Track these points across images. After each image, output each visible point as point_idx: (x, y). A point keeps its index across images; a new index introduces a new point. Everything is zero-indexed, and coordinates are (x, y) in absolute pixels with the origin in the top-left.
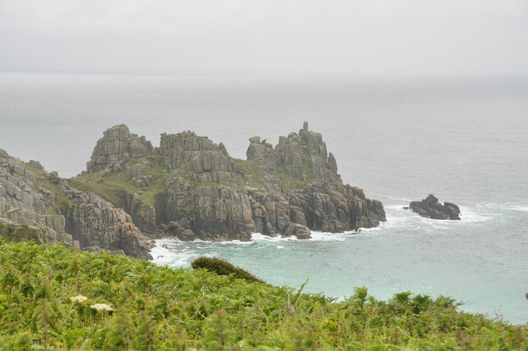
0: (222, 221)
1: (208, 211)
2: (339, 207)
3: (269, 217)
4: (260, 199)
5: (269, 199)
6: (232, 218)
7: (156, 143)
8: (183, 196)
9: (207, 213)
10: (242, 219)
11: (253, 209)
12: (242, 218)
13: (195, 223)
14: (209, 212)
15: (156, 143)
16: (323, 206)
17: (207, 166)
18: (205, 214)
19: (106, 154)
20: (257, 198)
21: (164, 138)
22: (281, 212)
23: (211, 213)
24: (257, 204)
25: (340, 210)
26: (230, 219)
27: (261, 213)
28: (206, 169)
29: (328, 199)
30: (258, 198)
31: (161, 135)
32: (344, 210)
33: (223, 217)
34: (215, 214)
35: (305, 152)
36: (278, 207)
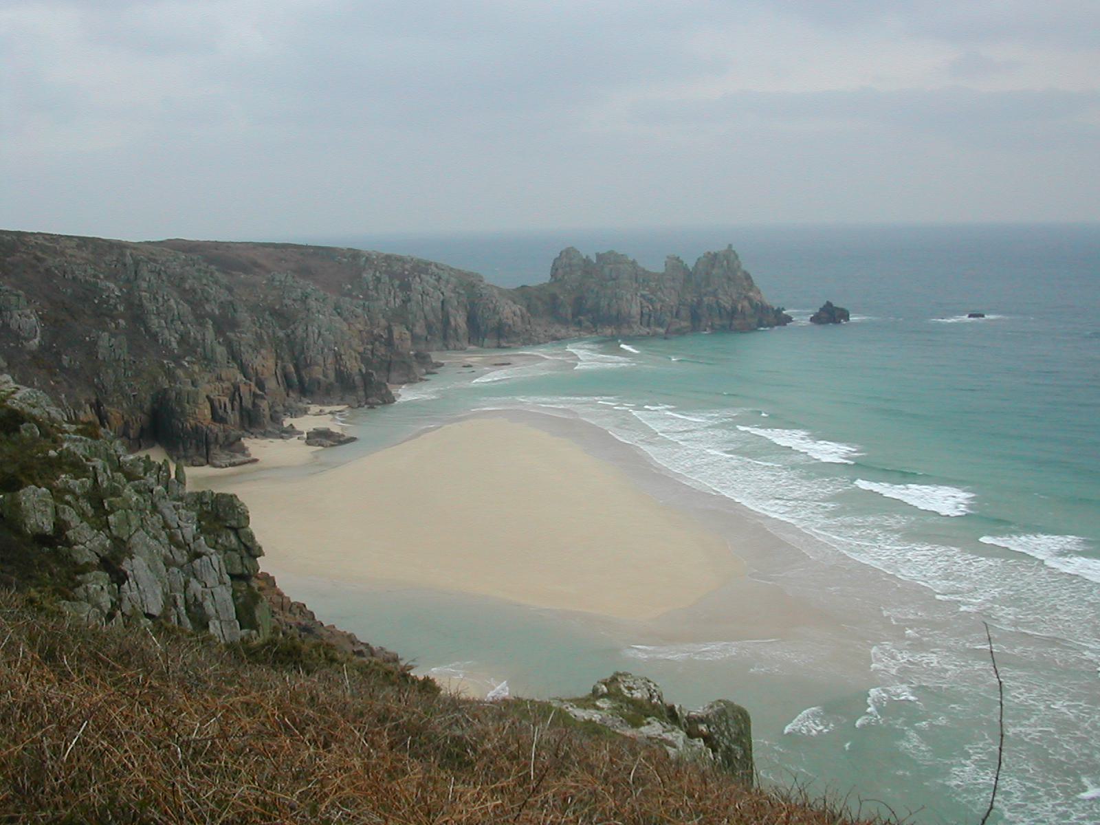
4: (650, 301)
11: (642, 307)
24: (645, 304)
33: (614, 313)
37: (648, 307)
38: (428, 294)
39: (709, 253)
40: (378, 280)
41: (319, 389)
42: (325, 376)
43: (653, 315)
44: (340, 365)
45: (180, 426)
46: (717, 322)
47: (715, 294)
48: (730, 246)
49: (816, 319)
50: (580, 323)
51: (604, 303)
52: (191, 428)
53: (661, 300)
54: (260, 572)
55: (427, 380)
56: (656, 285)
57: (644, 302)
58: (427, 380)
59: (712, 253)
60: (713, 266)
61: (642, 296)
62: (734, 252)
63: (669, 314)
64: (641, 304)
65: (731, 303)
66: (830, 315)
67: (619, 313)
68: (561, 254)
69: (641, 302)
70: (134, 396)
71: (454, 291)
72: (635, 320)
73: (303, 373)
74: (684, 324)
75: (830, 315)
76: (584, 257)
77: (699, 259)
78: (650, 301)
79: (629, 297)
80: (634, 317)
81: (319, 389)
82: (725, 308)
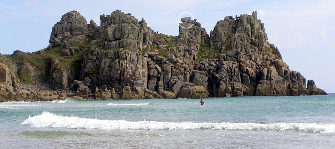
0: (115, 79)
1: (105, 70)
2: (244, 72)
3: (164, 76)
4: (160, 62)
5: (167, 62)
6: (124, 75)
7: (98, 23)
8: (92, 60)
9: (104, 73)
10: (132, 77)
11: (149, 69)
12: (134, 76)
13: (95, 82)
14: (106, 72)
15: (98, 23)
16: (228, 70)
17: (118, 35)
18: (103, 74)
19: (55, 34)
20: (157, 61)
21: (103, 19)
22: (176, 72)
23: (108, 72)
24: (153, 65)
25: (244, 75)
26: (122, 76)
27: (156, 72)
28: (116, 37)
29: (235, 65)
30: (158, 61)
31: (101, 16)
32: (249, 75)
33: (117, 75)
34: (111, 73)
35: (242, 31)
36: (174, 68)
37: (156, 68)
39: (231, 17)
43: (162, 77)
46: (238, 85)
47: (236, 57)
48: (255, 14)
51: (105, 64)
53: (171, 61)
54: (100, 26)
55: (276, 47)
56: (167, 48)
57: (151, 62)
58: (276, 47)
59: (234, 17)
60: (234, 30)
61: (150, 56)
62: (259, 21)
63: (182, 77)
64: (149, 65)
65: (255, 67)
67: (122, 73)
68: (62, 19)
69: (148, 62)
72: (140, 82)
74: (198, 88)
76: (89, 23)
77: (218, 23)
78: (160, 62)
79: (134, 57)
80: (140, 79)
82: (248, 73)
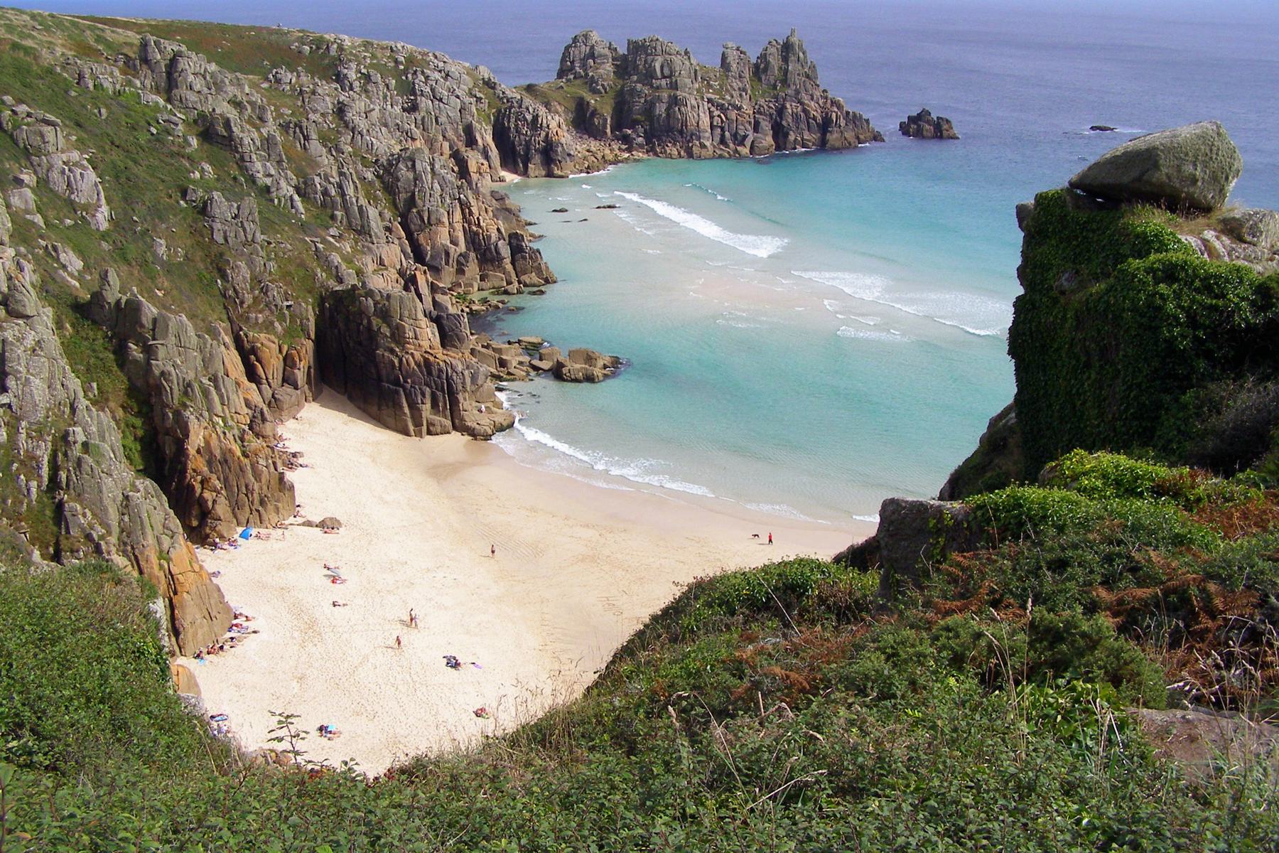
4: (721, 107)
11: (712, 117)
24: (716, 113)
38: (441, 100)
40: (367, 78)
41: (447, 263)
42: (454, 242)
44: (470, 224)
45: (396, 361)
49: (904, 129)
50: (626, 139)
52: (418, 365)
61: (710, 101)
66: (926, 128)
70: (288, 307)
71: (471, 95)
73: (422, 240)
75: (926, 128)
81: (447, 263)
82: (814, 118)
